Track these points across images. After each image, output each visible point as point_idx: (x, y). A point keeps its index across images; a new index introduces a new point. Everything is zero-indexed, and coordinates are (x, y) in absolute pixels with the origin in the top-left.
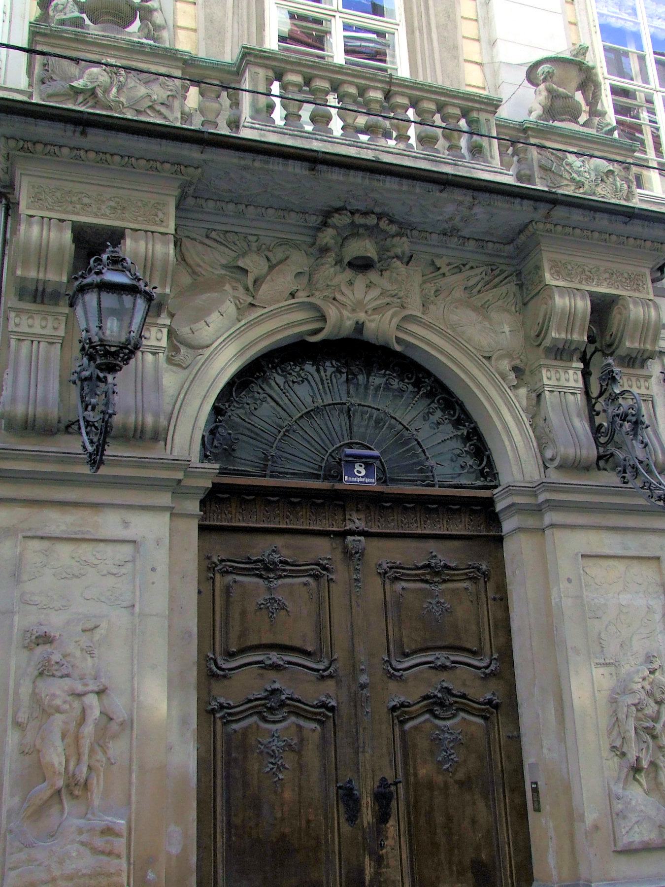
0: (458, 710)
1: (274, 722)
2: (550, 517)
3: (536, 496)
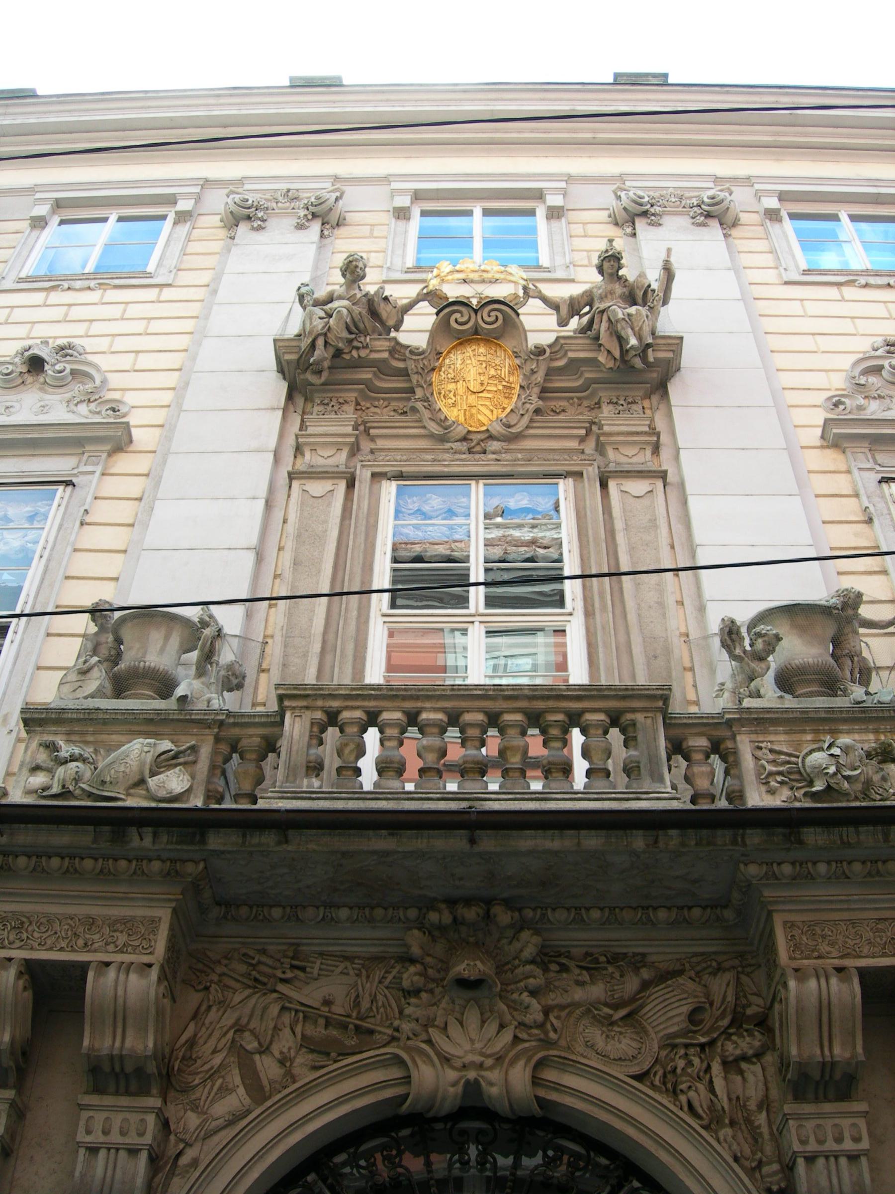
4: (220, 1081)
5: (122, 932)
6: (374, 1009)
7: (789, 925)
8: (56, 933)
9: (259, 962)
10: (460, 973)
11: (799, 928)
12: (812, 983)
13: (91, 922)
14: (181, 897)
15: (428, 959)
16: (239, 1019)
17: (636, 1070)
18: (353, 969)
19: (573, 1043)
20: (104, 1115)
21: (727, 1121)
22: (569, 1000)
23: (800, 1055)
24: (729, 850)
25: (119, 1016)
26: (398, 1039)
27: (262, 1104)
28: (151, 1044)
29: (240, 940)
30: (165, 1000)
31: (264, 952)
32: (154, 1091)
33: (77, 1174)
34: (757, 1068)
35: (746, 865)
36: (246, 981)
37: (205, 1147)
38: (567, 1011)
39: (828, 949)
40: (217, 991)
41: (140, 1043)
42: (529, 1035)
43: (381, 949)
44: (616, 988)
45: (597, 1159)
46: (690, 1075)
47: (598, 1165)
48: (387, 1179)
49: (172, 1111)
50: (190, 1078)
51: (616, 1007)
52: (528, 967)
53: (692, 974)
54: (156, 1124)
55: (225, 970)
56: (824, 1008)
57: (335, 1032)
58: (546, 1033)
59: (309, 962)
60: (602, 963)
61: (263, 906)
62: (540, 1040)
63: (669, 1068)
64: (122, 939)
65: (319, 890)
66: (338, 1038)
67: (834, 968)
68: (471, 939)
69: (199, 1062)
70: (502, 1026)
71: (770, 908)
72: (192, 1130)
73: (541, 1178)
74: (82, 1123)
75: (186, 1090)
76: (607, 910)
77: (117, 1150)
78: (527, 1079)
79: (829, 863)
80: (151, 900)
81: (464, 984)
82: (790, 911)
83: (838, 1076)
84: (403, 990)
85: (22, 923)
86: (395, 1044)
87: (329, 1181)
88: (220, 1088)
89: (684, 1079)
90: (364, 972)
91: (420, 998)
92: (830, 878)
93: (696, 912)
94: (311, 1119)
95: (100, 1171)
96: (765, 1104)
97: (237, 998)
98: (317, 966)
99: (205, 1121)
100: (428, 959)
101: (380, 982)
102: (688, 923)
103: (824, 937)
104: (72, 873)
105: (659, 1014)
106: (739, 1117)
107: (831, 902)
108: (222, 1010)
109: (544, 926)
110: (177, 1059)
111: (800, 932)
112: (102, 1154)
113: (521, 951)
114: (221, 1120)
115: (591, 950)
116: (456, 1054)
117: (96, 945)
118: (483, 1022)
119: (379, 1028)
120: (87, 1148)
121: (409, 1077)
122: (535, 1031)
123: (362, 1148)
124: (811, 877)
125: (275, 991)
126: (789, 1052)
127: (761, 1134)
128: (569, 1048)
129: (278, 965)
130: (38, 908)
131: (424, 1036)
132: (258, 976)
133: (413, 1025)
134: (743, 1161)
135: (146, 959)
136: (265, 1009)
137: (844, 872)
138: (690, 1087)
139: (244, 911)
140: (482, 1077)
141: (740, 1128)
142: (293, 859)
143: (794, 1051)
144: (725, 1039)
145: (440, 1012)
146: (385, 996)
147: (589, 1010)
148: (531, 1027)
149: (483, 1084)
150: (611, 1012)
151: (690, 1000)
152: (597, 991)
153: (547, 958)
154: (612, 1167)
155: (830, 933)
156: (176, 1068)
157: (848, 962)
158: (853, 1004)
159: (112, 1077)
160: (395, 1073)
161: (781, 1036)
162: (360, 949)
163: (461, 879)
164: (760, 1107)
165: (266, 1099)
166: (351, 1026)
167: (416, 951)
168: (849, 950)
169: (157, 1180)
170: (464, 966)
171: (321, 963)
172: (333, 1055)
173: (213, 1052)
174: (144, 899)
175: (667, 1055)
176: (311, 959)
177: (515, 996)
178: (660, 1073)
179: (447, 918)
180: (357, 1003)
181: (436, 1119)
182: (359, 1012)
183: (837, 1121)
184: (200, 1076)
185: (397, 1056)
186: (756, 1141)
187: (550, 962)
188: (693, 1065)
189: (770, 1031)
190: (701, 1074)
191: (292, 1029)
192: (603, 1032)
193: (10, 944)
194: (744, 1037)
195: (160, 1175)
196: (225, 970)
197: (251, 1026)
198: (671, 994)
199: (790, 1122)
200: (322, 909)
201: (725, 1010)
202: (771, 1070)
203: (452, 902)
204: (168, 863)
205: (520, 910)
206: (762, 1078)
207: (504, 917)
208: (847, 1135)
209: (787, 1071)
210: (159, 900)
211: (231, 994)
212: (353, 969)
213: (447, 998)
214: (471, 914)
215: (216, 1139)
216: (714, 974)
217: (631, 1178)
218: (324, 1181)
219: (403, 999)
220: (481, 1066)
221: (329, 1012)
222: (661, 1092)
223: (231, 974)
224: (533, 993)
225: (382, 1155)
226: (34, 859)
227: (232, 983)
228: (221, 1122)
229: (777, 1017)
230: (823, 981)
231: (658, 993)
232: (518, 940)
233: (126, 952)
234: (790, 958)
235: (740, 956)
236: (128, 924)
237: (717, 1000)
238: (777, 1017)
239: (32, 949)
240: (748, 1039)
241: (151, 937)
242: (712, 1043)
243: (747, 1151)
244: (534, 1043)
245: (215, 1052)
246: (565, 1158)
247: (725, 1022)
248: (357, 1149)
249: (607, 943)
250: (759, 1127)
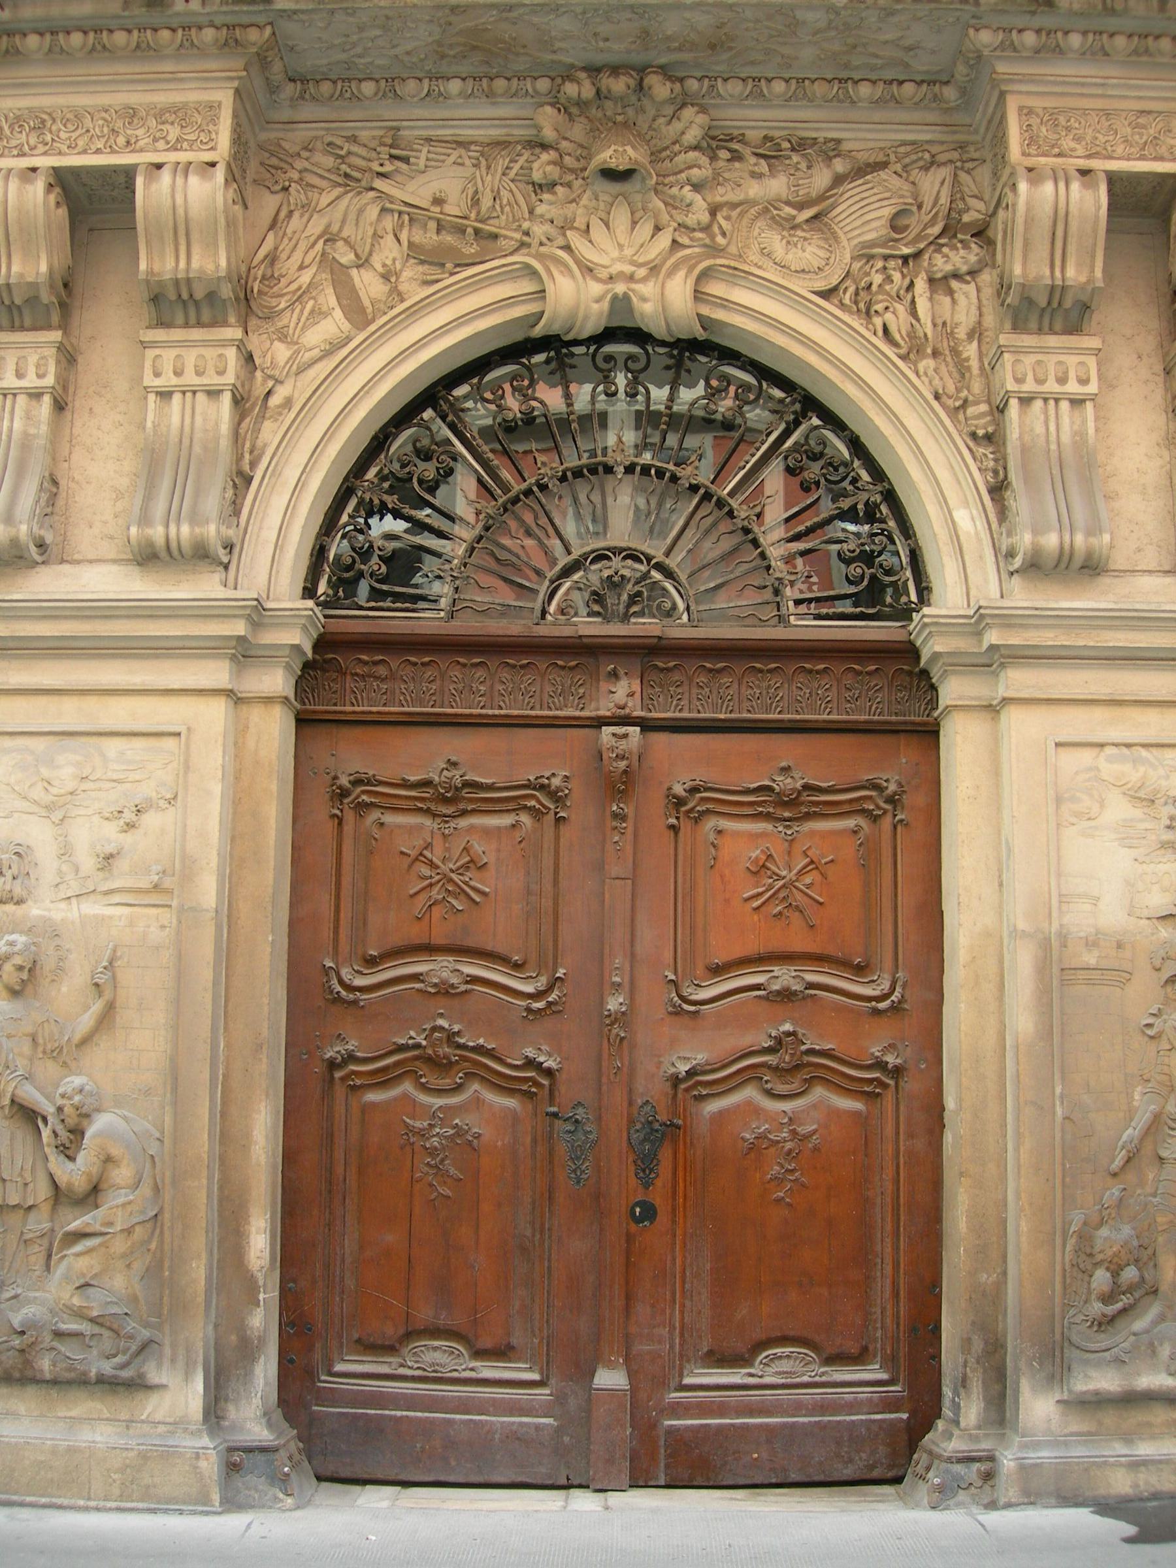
0: (469, 1076)
1: (440, 1092)
2: (1018, 680)
3: (979, 634)
4: (311, 303)
5: (172, 123)
6: (498, 207)
7: (1025, 111)
8: (88, 131)
9: (349, 153)
10: (605, 162)
11: (1038, 115)
12: (1048, 188)
13: (131, 114)
14: (245, 73)
15: (564, 144)
16: (329, 226)
17: (821, 285)
18: (470, 157)
19: (746, 250)
20: (173, 353)
21: (929, 351)
22: (742, 197)
23: (1024, 275)
24: (957, 9)
25: (181, 231)
26: (529, 245)
27: (364, 329)
28: (223, 263)
29: (323, 125)
30: (236, 207)
31: (353, 139)
32: (232, 320)
33: (149, 424)
34: (971, 288)
35: (977, 30)
36: (332, 177)
37: (299, 384)
38: (738, 210)
39: (1073, 145)
40: (299, 192)
41: (210, 262)
42: (691, 239)
43: (504, 131)
44: (801, 182)
45: (770, 391)
46: (888, 294)
47: (771, 398)
48: (519, 415)
49: (255, 343)
50: (274, 302)
51: (800, 206)
52: (692, 155)
53: (898, 167)
54: (238, 359)
55: (306, 165)
56: (1060, 219)
57: (448, 238)
58: (712, 237)
60: (785, 149)
61: (349, 80)
62: (705, 246)
63: (863, 284)
64: (173, 133)
65: (422, 56)
66: (457, 245)
67: (1078, 170)
68: (620, 118)
69: (283, 281)
70: (658, 229)
71: (1004, 88)
72: (282, 364)
73: (701, 413)
74: (148, 364)
75: (270, 316)
76: (794, 81)
77: (194, 392)
78: (688, 293)
79: (1085, 33)
80: (206, 79)
81: (611, 175)
82: (1028, 93)
83: (1068, 304)
84: (533, 184)
85: (43, 122)
86: (524, 251)
87: (450, 418)
88: (312, 312)
89: (880, 297)
90: (483, 162)
91: (555, 193)
92: (1084, 54)
93: (909, 88)
94: (425, 345)
95: (175, 420)
96: (977, 332)
97: (325, 200)
98: (423, 155)
99: (297, 352)
100: (564, 144)
101: (504, 174)
102: (897, 102)
103: (1068, 129)
104: (100, 52)
105: (854, 217)
106: (944, 346)
107: (1083, 85)
108: (307, 216)
109: (712, 102)
110: (255, 279)
111: (1039, 121)
112: (177, 398)
113: (683, 133)
114: (317, 351)
115: (771, 133)
116: (602, 262)
117: (141, 143)
118: (634, 223)
119: (503, 232)
120: (157, 393)
121: (544, 291)
123: (487, 379)
124: (1059, 51)
125: (372, 189)
126: (1011, 271)
127: (969, 368)
128: (740, 256)
129: (374, 155)
130: (61, 100)
131: (561, 241)
132: (348, 171)
133: (547, 227)
134: (944, 399)
135: (208, 157)
136: (361, 211)
137: (1103, 48)
138: (887, 308)
139: (326, 87)
140: (633, 291)
141: (944, 360)
142: (388, 18)
143: (1018, 270)
144: (935, 251)
145: (580, 211)
146: (511, 191)
147: (767, 209)
148: (694, 230)
149: (634, 299)
150: (794, 212)
151: (893, 201)
152: (777, 186)
153: (718, 143)
154: (788, 400)
155: (1077, 125)
156: (255, 291)
157: (1095, 164)
158: (1097, 217)
159: (177, 305)
160: (527, 286)
161: (1004, 250)
162: (482, 132)
163: (607, 40)
164: (970, 336)
165: (369, 323)
166: (470, 230)
167: (549, 134)
168: (1098, 149)
169: (244, 425)
170: (610, 152)
171: (429, 152)
172: (449, 266)
173: (299, 269)
174: (197, 79)
175: (861, 268)
176: (415, 146)
177: (675, 190)
178: (852, 290)
179: (588, 91)
180: (476, 202)
181: (576, 343)
182: (478, 213)
183: (1062, 358)
184: (286, 298)
185: (527, 266)
186: (963, 376)
188: (892, 281)
189: (991, 243)
190: (902, 292)
191: (396, 236)
192: (783, 237)
193: (31, 149)
194: (957, 249)
195: (248, 420)
196: (306, 165)
197: (345, 234)
198: (871, 192)
199: (1006, 355)
200: (426, 82)
201: (937, 214)
202: (988, 292)
203: (594, 70)
204: (225, 30)
205: (681, 80)
206: (975, 301)
207: (661, 89)
208: (1072, 375)
209: (1007, 293)
210: (216, 79)
211: (316, 195)
212: (470, 157)
213: (588, 193)
214: (619, 85)
215: (311, 373)
216: (926, 168)
217: (810, 414)
218: (443, 418)
219: (533, 195)
220: (631, 278)
221: (441, 213)
222: (851, 313)
223: (315, 169)
224: (697, 187)
225: (512, 385)
226: (48, 37)
227: (315, 181)
228: (316, 353)
229: (1000, 227)
230: (1062, 185)
231: (853, 191)
232: (679, 119)
233: (181, 149)
234: (1024, 154)
235: (961, 147)
236: (180, 115)
237: (928, 203)
238: (1000, 227)
239: (60, 153)
240: (962, 252)
241: (211, 127)
242: (917, 255)
243: (951, 389)
244: (697, 250)
245: (301, 268)
246: (732, 389)
247: (936, 230)
248: (481, 380)
249: (792, 125)
250: (968, 359)
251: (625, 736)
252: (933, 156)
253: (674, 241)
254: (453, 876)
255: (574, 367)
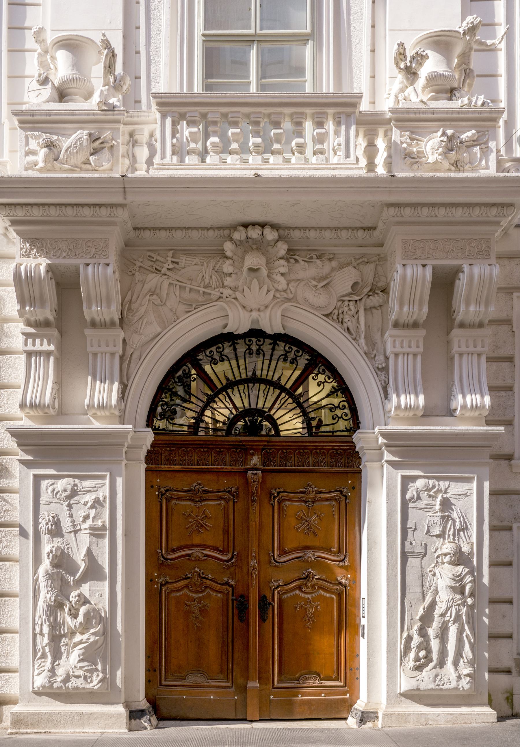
7: (404, 241)
9: (157, 260)
55: (141, 264)
59: (179, 259)
86: (221, 300)
101: (213, 269)
122: (283, 293)
125: (165, 275)
172: (194, 306)
175: (340, 305)
178: (336, 314)
187: (291, 258)
240: (377, 298)
251: (256, 474)
252: (368, 260)
253: (274, 296)
254: (200, 521)
255: (238, 344)
